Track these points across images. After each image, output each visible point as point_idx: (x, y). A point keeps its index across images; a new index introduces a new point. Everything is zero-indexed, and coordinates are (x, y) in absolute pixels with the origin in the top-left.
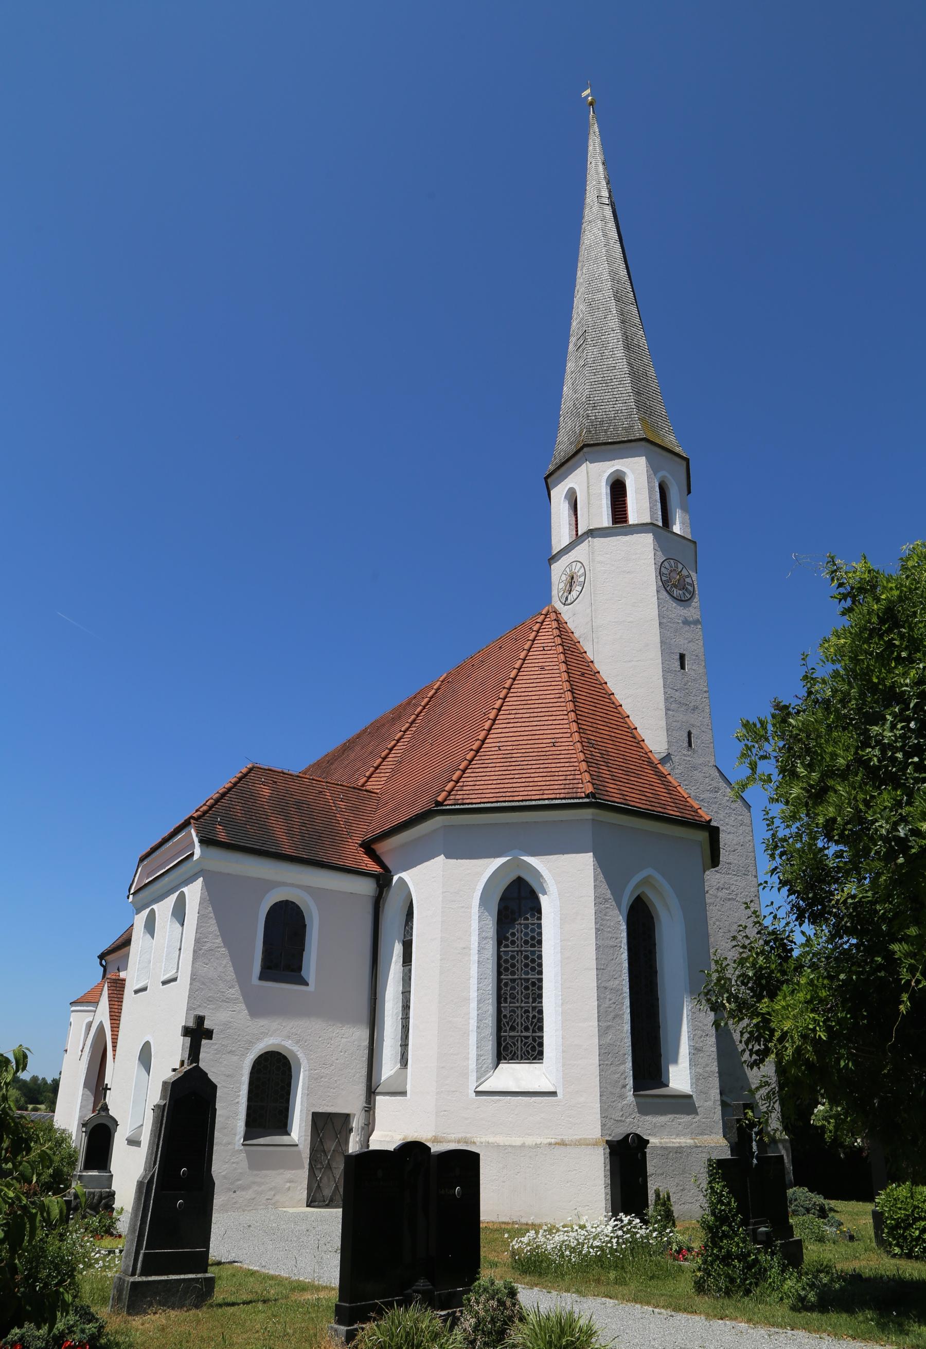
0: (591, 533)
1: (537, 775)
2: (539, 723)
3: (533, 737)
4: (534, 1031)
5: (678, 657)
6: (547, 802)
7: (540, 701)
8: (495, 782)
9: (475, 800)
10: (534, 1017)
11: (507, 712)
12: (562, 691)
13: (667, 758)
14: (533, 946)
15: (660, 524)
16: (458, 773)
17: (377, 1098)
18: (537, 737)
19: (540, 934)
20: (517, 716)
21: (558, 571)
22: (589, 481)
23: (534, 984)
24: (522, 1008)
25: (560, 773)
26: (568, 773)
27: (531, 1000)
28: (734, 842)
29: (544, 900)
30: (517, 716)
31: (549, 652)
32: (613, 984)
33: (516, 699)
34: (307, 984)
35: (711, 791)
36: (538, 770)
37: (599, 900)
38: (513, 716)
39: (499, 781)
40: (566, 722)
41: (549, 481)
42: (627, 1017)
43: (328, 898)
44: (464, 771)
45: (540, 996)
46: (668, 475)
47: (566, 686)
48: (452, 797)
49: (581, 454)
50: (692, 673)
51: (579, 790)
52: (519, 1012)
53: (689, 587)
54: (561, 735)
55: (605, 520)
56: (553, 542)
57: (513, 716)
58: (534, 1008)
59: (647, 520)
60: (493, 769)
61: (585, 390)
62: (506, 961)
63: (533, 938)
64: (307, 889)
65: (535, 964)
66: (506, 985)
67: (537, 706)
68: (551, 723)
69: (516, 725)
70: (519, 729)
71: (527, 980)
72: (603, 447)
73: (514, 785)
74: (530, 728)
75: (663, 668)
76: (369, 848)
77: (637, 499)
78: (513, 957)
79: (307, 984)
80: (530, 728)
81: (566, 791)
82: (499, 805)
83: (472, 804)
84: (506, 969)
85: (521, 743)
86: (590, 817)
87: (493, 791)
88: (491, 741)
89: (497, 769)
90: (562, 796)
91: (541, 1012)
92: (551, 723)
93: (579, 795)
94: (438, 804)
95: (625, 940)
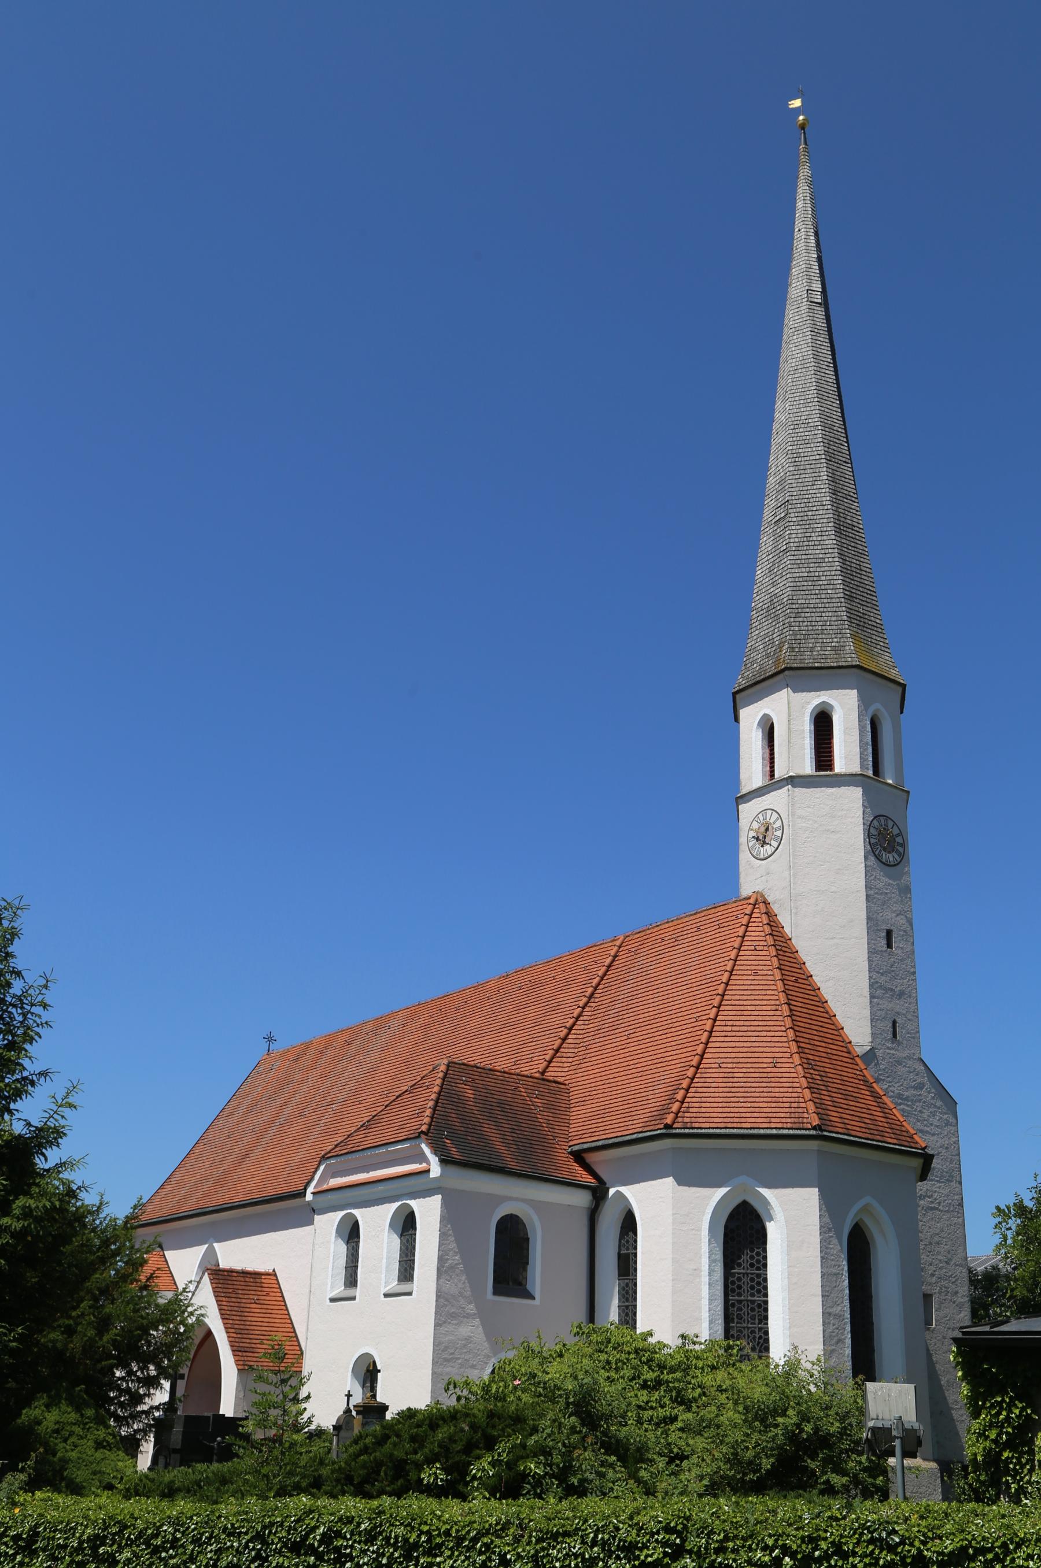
0: (794, 781)
1: (762, 1100)
2: (757, 1039)
3: (753, 1055)
5: (884, 934)
6: (774, 1131)
7: (757, 1013)
8: (720, 1105)
9: (704, 1125)
10: (760, 1338)
11: (723, 1023)
12: (777, 1003)
13: (870, 1056)
14: (758, 1269)
15: (870, 773)
16: (682, 1093)
18: (756, 1055)
19: (765, 1258)
20: (734, 1028)
21: (748, 811)
22: (789, 709)
23: (759, 1306)
24: (748, 1328)
25: (785, 1100)
26: (792, 1100)
27: (757, 1321)
28: (938, 1144)
29: (771, 1228)
30: (734, 1028)
31: (761, 953)
32: (836, 1310)
33: (730, 1008)
34: (534, 1298)
35: (915, 1088)
36: (762, 1095)
37: (824, 1229)
38: (729, 1028)
39: (725, 1105)
40: (785, 1039)
41: (739, 698)
42: (848, 1341)
43: (548, 1209)
44: (687, 1090)
45: (766, 1318)
46: (883, 710)
47: (783, 998)
48: (680, 1120)
49: (781, 676)
50: (899, 952)
51: (805, 1120)
54: (781, 1055)
55: (807, 767)
56: (743, 776)
57: (729, 1028)
58: (760, 1329)
59: (856, 769)
60: (716, 1090)
61: (784, 589)
62: (733, 1283)
63: (758, 1261)
64: (531, 1203)
66: (733, 1305)
67: (753, 1018)
68: (769, 1039)
69: (733, 1039)
70: (737, 1044)
71: (753, 1302)
73: (741, 1110)
74: (749, 1044)
76: (579, 1157)
78: (739, 1279)
79: (534, 1298)
80: (749, 1044)
81: (792, 1120)
82: (727, 1131)
83: (701, 1128)
84: (733, 1291)
85: (741, 1060)
86: (816, 1148)
87: (720, 1115)
88: (710, 1055)
89: (721, 1090)
90: (789, 1125)
91: (767, 1333)
92: (769, 1039)
93: (805, 1126)
94: (667, 1126)
95: (846, 1268)
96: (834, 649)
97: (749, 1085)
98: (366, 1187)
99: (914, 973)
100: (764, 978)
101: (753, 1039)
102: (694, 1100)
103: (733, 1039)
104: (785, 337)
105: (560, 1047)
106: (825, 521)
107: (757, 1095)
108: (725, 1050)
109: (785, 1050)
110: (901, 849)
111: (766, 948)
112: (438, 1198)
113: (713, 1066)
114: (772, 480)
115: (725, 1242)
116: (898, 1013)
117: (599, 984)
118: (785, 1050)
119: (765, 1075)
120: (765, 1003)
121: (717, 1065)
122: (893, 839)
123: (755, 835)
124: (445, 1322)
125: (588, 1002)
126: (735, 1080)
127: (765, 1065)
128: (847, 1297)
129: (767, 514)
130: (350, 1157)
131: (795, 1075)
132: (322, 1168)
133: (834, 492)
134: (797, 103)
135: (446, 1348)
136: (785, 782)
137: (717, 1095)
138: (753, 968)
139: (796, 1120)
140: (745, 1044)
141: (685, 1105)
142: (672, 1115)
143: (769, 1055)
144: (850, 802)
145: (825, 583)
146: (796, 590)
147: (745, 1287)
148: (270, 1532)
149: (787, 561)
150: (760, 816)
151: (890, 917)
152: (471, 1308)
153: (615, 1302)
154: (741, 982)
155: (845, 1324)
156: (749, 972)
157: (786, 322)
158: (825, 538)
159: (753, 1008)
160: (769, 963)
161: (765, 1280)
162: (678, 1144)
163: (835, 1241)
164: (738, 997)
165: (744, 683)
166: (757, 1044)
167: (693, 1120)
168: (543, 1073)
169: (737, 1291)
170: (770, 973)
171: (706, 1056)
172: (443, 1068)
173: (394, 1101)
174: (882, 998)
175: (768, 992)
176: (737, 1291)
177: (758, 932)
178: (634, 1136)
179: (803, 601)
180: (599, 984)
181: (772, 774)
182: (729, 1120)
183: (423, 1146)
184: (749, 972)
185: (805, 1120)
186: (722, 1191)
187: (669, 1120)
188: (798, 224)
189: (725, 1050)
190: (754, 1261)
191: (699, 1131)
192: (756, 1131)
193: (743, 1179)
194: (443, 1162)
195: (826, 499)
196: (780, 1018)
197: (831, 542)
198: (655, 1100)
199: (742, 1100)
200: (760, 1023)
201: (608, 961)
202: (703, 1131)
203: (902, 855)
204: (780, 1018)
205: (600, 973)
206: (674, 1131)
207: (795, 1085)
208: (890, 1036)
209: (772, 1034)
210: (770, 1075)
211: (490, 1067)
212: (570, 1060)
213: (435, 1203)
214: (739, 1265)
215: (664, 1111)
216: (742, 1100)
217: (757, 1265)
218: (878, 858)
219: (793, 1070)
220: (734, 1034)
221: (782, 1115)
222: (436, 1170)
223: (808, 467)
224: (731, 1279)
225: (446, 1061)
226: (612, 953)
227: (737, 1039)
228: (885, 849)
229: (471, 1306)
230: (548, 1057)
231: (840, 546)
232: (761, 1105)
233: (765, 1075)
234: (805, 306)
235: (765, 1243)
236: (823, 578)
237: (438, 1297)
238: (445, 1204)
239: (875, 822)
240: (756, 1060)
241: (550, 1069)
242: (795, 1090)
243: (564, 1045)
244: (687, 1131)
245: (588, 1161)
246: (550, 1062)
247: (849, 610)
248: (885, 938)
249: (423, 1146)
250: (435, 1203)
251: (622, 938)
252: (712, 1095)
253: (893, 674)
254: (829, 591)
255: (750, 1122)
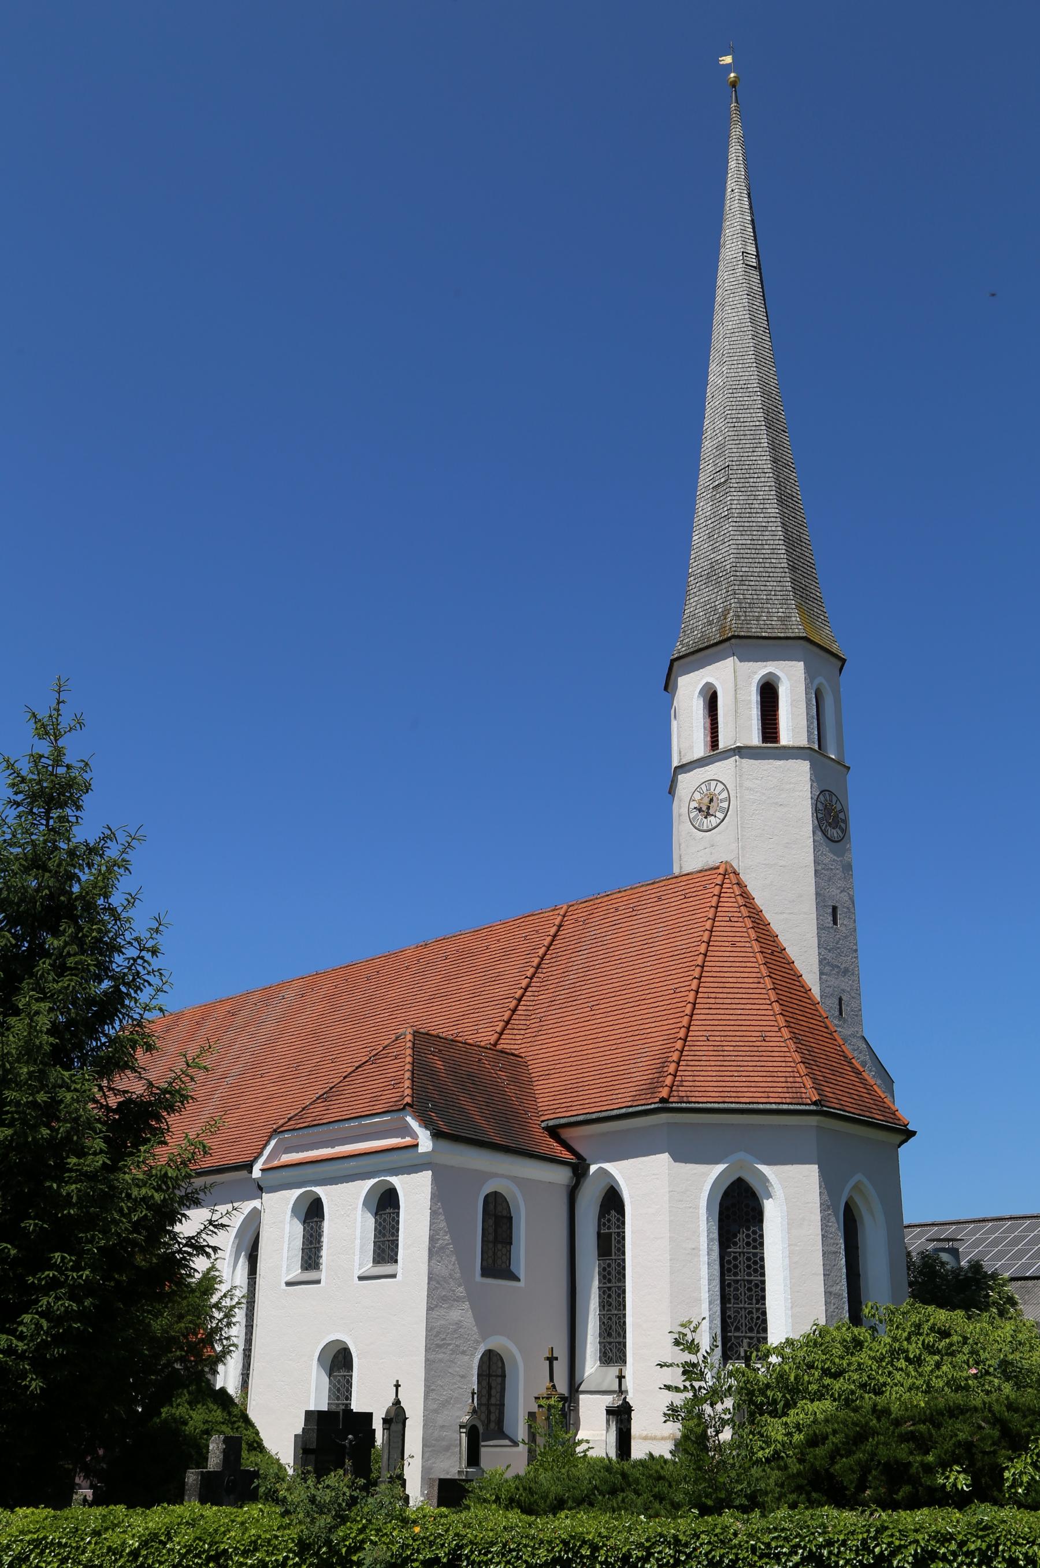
0: (741, 751)
4: (758, 1332)
5: (830, 910)
6: (774, 1106)
10: (758, 1318)
11: (706, 995)
12: (759, 975)
14: (755, 1248)
15: (816, 747)
16: (673, 1066)
17: (581, 1397)
20: (718, 1001)
21: (687, 783)
22: (734, 679)
23: (757, 1286)
24: (745, 1309)
25: (780, 1074)
26: (787, 1074)
27: (754, 1301)
30: (718, 1001)
31: (736, 924)
32: (836, 1289)
34: (519, 1280)
36: (756, 1069)
38: (713, 1001)
43: (530, 1185)
45: (764, 1298)
49: (727, 644)
50: (843, 929)
52: (743, 1313)
53: (842, 825)
54: (769, 1029)
55: (754, 738)
57: (713, 1001)
58: (758, 1309)
59: (803, 742)
60: (708, 1063)
61: (726, 555)
62: (729, 1262)
64: (514, 1179)
65: (757, 1266)
67: (736, 990)
70: (723, 1017)
72: (754, 641)
73: (736, 1084)
74: (735, 1017)
75: (818, 924)
76: (553, 1132)
77: (792, 714)
78: (735, 1259)
79: (519, 1280)
80: (735, 1017)
81: (791, 1095)
82: (726, 1106)
83: (698, 1103)
86: (815, 1124)
88: (696, 1028)
90: (788, 1100)
91: (764, 1313)
94: (663, 1100)
95: (843, 1247)
96: (780, 619)
97: (741, 1058)
98: (333, 1162)
99: (856, 951)
100: (743, 949)
101: (739, 1012)
102: (686, 1073)
103: (718, 1011)
104: (718, 299)
105: (510, 1019)
106: (767, 488)
107: (751, 1069)
108: (711, 1023)
109: (773, 1023)
110: (842, 825)
111: (741, 919)
112: (427, 1175)
113: (701, 1039)
114: (708, 445)
115: (720, 1220)
116: (843, 990)
117: (545, 954)
118: (773, 1023)
119: (756, 1049)
120: (746, 975)
121: (705, 1038)
122: (836, 817)
123: (697, 805)
124: (436, 1306)
125: (535, 973)
126: (726, 1053)
127: (754, 1039)
128: (844, 1276)
129: (703, 479)
130: (310, 1130)
131: (786, 1049)
132: (273, 1143)
133: (775, 461)
134: (728, 60)
135: (438, 1333)
136: (732, 753)
137: (709, 1068)
138: (730, 939)
139: (795, 1095)
140: (731, 1017)
141: (677, 1078)
142: (667, 1089)
143: (757, 1028)
144: (799, 774)
145: (769, 551)
146: (739, 557)
147: (741, 1267)
148: (830, 1553)
149: (728, 527)
150: (703, 786)
151: (835, 894)
152: (461, 1291)
153: (596, 1283)
154: (720, 954)
155: (844, 1303)
156: (727, 944)
157: (719, 283)
158: (767, 506)
159: (734, 980)
160: (745, 934)
161: (762, 1259)
162: (670, 1118)
163: (833, 1219)
164: (718, 969)
165: (684, 650)
166: (743, 1017)
167: (689, 1094)
168: (495, 1045)
169: (734, 1270)
170: (747, 945)
171: (692, 1028)
172: (409, 1037)
173: (353, 1071)
174: (829, 975)
175: (748, 964)
176: (734, 1270)
177: (730, 904)
178: (623, 1111)
179: (747, 569)
180: (545, 954)
181: (714, 743)
182: (726, 1094)
183: (409, 1119)
184: (727, 944)
185: (804, 1095)
186: (720, 1168)
187: (664, 1093)
188: (731, 184)
189: (711, 1023)
190: (750, 1240)
191: (697, 1105)
192: (755, 1106)
193: (741, 1155)
194: (437, 1135)
195: (768, 466)
196: (764, 991)
197: (773, 511)
198: (640, 1072)
199: (736, 1074)
200: (744, 996)
201: (553, 930)
202: (701, 1105)
203: (844, 831)
204: (764, 991)
205: (546, 943)
206: (671, 1105)
207: (787, 1059)
208: (837, 1013)
209: (758, 1007)
210: (760, 1049)
211: (451, 1037)
212: (523, 1032)
213: (425, 1178)
214: (735, 1244)
215: (654, 1085)
216: (736, 1074)
217: (753, 1244)
218: (824, 833)
219: (783, 1044)
220: (718, 1006)
221: (780, 1090)
222: (425, 1142)
223: (748, 433)
224: (727, 1258)
225: (410, 1030)
226: (557, 922)
227: (722, 1012)
228: (830, 824)
229: (461, 1289)
230: (498, 1029)
231: (782, 514)
232: (756, 1079)
233: (756, 1049)
234: (740, 269)
235: (761, 1221)
236: (766, 547)
237: (430, 1279)
238: (435, 1180)
239: (821, 796)
240: (744, 1033)
241: (502, 1041)
242: (789, 1064)
243: (514, 1017)
244: (684, 1105)
245: (563, 1136)
246: (501, 1034)
247: (793, 581)
248: (832, 914)
249: (409, 1119)
250: (425, 1178)
251: (565, 907)
252: (704, 1068)
253: (835, 648)
254: (773, 561)
255: (747, 1097)
